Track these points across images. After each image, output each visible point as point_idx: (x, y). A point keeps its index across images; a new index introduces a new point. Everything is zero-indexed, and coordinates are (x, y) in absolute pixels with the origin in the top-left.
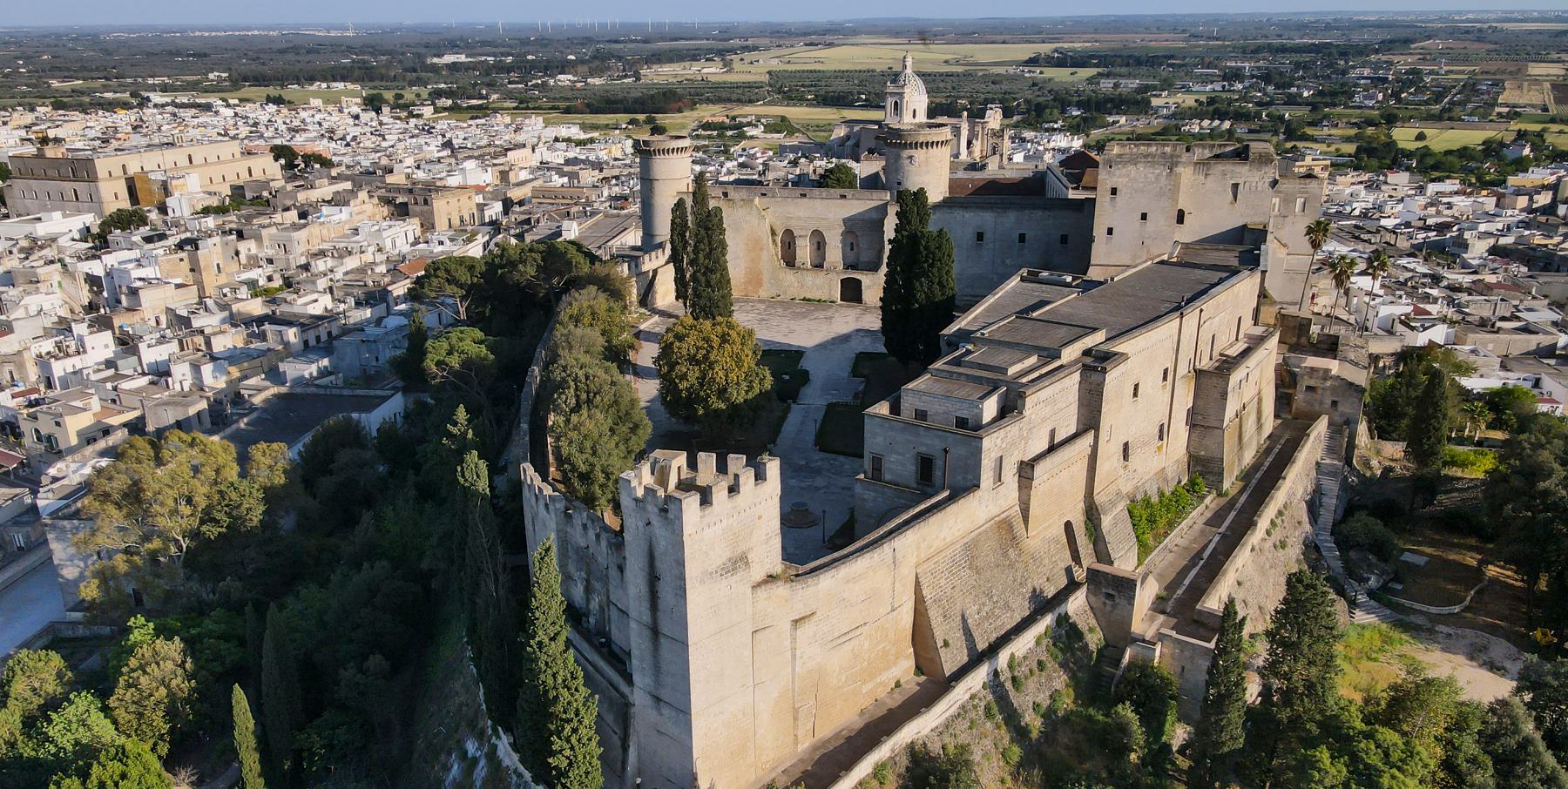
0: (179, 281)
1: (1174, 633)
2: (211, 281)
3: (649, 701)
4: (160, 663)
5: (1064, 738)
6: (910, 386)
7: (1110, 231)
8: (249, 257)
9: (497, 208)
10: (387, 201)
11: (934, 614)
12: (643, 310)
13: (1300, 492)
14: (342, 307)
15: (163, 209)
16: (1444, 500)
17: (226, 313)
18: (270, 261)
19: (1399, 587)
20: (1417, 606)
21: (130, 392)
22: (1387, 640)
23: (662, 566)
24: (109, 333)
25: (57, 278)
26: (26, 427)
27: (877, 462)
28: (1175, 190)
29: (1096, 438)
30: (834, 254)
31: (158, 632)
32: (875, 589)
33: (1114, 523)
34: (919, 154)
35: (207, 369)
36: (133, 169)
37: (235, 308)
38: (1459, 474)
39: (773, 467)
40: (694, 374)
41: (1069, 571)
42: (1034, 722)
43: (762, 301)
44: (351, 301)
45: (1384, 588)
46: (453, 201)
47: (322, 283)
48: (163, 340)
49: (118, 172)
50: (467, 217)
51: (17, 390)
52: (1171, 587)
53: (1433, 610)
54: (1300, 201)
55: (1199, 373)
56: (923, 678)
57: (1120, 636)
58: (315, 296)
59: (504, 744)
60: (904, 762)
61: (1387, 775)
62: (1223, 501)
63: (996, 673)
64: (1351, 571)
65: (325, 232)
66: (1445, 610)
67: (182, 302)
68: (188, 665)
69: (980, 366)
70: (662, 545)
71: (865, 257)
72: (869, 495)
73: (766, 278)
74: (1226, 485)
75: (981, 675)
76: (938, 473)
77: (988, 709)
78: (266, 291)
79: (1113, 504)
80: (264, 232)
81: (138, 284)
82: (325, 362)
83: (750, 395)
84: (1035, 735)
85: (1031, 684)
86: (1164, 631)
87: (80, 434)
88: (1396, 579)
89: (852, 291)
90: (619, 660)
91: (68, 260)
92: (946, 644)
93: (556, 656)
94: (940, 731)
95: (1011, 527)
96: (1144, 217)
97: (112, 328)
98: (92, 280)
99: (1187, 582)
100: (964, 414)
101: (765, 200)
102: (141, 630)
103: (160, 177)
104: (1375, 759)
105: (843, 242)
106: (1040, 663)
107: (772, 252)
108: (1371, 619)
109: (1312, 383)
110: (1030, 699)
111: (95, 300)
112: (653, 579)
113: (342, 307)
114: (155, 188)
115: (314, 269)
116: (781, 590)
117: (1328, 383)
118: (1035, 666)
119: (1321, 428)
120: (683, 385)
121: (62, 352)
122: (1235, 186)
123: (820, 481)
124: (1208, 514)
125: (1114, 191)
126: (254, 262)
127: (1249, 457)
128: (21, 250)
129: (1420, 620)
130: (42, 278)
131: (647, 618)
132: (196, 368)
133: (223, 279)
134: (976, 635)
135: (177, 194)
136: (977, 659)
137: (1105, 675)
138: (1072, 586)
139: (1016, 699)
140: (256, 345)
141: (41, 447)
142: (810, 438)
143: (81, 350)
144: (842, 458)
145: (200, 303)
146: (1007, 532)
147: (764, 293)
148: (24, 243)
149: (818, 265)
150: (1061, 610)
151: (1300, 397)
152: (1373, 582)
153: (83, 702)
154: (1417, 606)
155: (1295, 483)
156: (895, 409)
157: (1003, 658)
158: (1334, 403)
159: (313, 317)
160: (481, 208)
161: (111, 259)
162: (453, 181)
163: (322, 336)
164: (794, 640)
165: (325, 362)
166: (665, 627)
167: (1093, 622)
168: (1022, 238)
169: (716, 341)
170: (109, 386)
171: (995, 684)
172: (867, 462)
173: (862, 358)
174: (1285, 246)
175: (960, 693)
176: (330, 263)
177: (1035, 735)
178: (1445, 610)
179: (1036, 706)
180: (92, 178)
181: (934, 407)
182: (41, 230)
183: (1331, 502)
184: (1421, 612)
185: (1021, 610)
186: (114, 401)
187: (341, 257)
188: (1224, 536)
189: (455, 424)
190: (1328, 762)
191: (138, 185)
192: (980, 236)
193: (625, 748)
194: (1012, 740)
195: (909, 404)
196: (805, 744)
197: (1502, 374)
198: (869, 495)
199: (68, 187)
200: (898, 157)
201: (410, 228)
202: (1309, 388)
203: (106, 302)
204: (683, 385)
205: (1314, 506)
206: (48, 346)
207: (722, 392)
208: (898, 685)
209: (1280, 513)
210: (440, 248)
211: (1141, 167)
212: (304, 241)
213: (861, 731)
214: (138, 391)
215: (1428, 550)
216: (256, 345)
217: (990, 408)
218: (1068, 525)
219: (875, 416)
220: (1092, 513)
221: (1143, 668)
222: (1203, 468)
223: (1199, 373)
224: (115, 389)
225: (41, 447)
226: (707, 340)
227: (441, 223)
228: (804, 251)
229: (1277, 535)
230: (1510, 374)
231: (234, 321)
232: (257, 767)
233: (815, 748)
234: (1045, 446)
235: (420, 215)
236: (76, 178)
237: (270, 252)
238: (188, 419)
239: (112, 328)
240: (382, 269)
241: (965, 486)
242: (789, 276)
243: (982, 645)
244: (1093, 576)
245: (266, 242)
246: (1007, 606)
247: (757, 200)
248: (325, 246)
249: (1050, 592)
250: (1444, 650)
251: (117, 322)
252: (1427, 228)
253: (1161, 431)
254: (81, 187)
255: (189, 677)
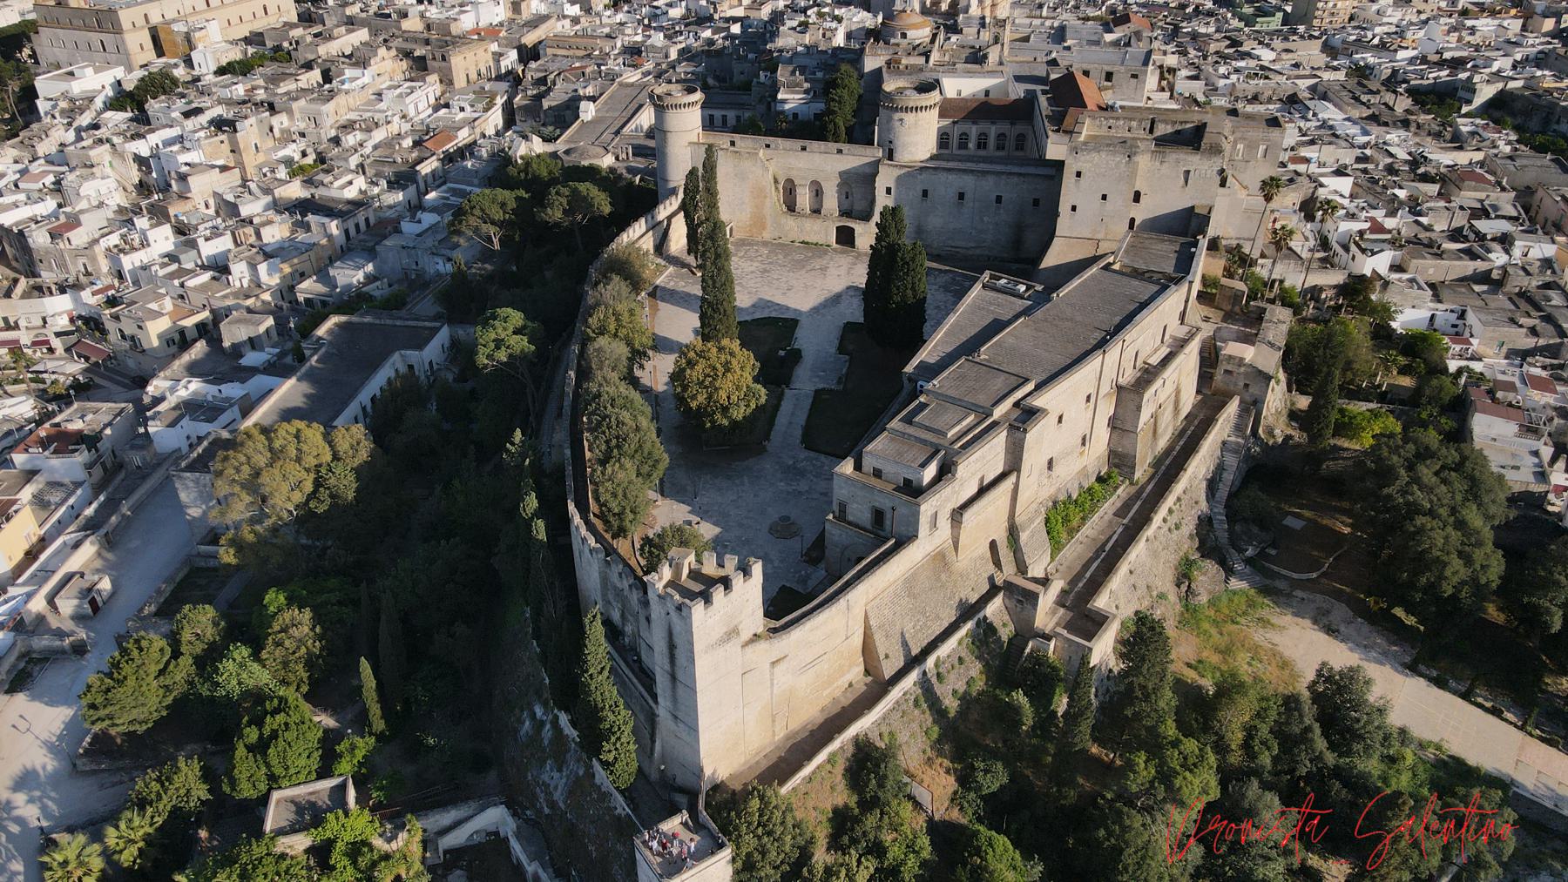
0: (221, 162)
1: (1065, 632)
2: (251, 161)
3: (669, 716)
4: (297, 627)
5: (974, 716)
6: (870, 447)
7: (1074, 208)
8: (282, 131)
9: (511, 59)
10: (407, 54)
11: (879, 639)
12: (659, 261)
13: (1203, 471)
14: (376, 190)
15: (189, 62)
16: (1329, 466)
17: (269, 198)
18: (303, 135)
19: (1273, 552)
20: (1284, 572)
21: (196, 289)
22: (1251, 604)
23: (678, 640)
24: (168, 226)
25: (108, 158)
26: (110, 325)
27: (843, 507)
28: (1133, 175)
29: (1018, 477)
30: (831, 202)
31: (290, 601)
32: (828, 647)
33: (1033, 537)
34: (909, 118)
35: (263, 268)
36: (155, 19)
37: (277, 192)
38: (1346, 445)
39: (757, 569)
40: (701, 398)
41: (991, 579)
42: (951, 704)
43: (765, 244)
44: (383, 183)
45: (1262, 554)
46: (470, 55)
47: (354, 161)
48: (216, 233)
49: (141, 22)
50: (483, 71)
51: (95, 288)
52: (1073, 582)
53: (1295, 576)
54: (1262, 148)
55: (1120, 388)
56: (870, 679)
57: (1025, 632)
58: (349, 177)
59: (564, 719)
60: (850, 750)
61: (1180, 778)
62: (1133, 490)
63: (925, 673)
64: (1235, 542)
65: (351, 101)
66: (1304, 576)
67: (226, 184)
68: (318, 630)
69: (928, 429)
70: (678, 627)
71: (859, 206)
72: (836, 532)
73: (769, 222)
74: (1138, 475)
75: (914, 676)
76: (888, 522)
77: (916, 701)
78: (302, 169)
79: (1031, 520)
80: (295, 105)
81: (184, 169)
82: (370, 268)
83: (749, 411)
84: (952, 714)
85: (952, 677)
86: (1059, 630)
87: (160, 336)
88: (1274, 545)
89: (846, 237)
90: (647, 678)
91: (116, 140)
92: (887, 657)
93: (602, 686)
94: (877, 724)
95: (944, 556)
96: (1104, 197)
97: (167, 218)
98: (140, 161)
99: (1088, 575)
100: (909, 477)
101: (768, 151)
102: (274, 598)
103: (180, 28)
104: (1175, 765)
105: (839, 192)
106: (960, 659)
107: (775, 199)
108: (1243, 585)
109: (1229, 368)
110: (950, 688)
111: (145, 179)
112: (672, 647)
113: (376, 190)
114: (179, 39)
115: (344, 143)
116: (762, 645)
117: (1242, 369)
118: (956, 662)
119: (1233, 408)
120: (694, 405)
121: (127, 247)
122: (1187, 172)
123: (803, 486)
124: (1119, 504)
125: (1079, 174)
126: (287, 138)
127: (1162, 443)
128: (63, 112)
129: (1281, 585)
130: (94, 161)
131: (667, 667)
132: (253, 267)
133: (261, 158)
134: (911, 644)
135: (200, 46)
136: (913, 661)
137: (1011, 663)
138: (993, 590)
139: (939, 689)
140: (301, 236)
141: (126, 345)
142: (798, 433)
143: (145, 244)
144: (823, 457)
145: (244, 186)
146: (940, 560)
147: (767, 235)
148: (63, 104)
149: (817, 211)
150: (981, 615)
151: (1219, 376)
152: (1250, 552)
153: (241, 652)
154: (1284, 572)
155: (1199, 467)
156: (858, 467)
157: (930, 662)
158: (1246, 386)
159: (349, 202)
160: (498, 57)
161: (155, 138)
162: (467, 22)
163: (367, 232)
164: (772, 674)
165: (370, 268)
166: (680, 675)
167: (1007, 618)
168: (999, 199)
169: (721, 369)
170: (176, 282)
171: (924, 683)
172: (835, 508)
173: (849, 328)
174: (1246, 188)
175: (896, 693)
176: (359, 136)
177: (952, 714)
178: (1304, 576)
179: (955, 692)
180: (117, 29)
181: (888, 469)
182: (77, 88)
183: (1228, 477)
184: (1286, 578)
185: (949, 616)
186: (182, 297)
187: (369, 130)
188: (1127, 527)
189: (513, 444)
190: (1142, 765)
191: (162, 36)
192: (961, 196)
193: (653, 742)
194: (935, 722)
195: (868, 463)
196: (781, 734)
197: (1432, 305)
198: (836, 532)
199: (95, 38)
200: (890, 119)
201: (430, 89)
202: (1226, 371)
203: (156, 190)
204: (694, 405)
205: (1212, 485)
206: (114, 239)
207: (725, 410)
208: (850, 685)
209: (1179, 499)
210: (461, 115)
211: (1103, 155)
212: (333, 113)
213: (822, 725)
214: (202, 288)
215: (1307, 513)
216: (301, 236)
217: (930, 472)
218: (993, 545)
219: (841, 475)
220: (1013, 532)
221: (1039, 659)
222: (1120, 461)
223: (1120, 388)
224: (182, 285)
225: (126, 345)
226: (714, 368)
227: (460, 82)
228: (804, 199)
229: (1173, 520)
230: (1440, 306)
231: (279, 207)
232: (379, 712)
233: (788, 738)
234: (974, 490)
235: (439, 71)
236: (100, 27)
237: (302, 126)
238: (259, 336)
239: (167, 218)
240: (407, 143)
241: (904, 541)
242: (790, 222)
243: (915, 651)
244: (1009, 587)
245: (297, 115)
246: (938, 617)
247: (761, 153)
248: (353, 116)
249: (974, 598)
250: (1296, 615)
251: (172, 211)
252: (1442, 64)
253: (1084, 439)
254: (108, 39)
255: (320, 638)
